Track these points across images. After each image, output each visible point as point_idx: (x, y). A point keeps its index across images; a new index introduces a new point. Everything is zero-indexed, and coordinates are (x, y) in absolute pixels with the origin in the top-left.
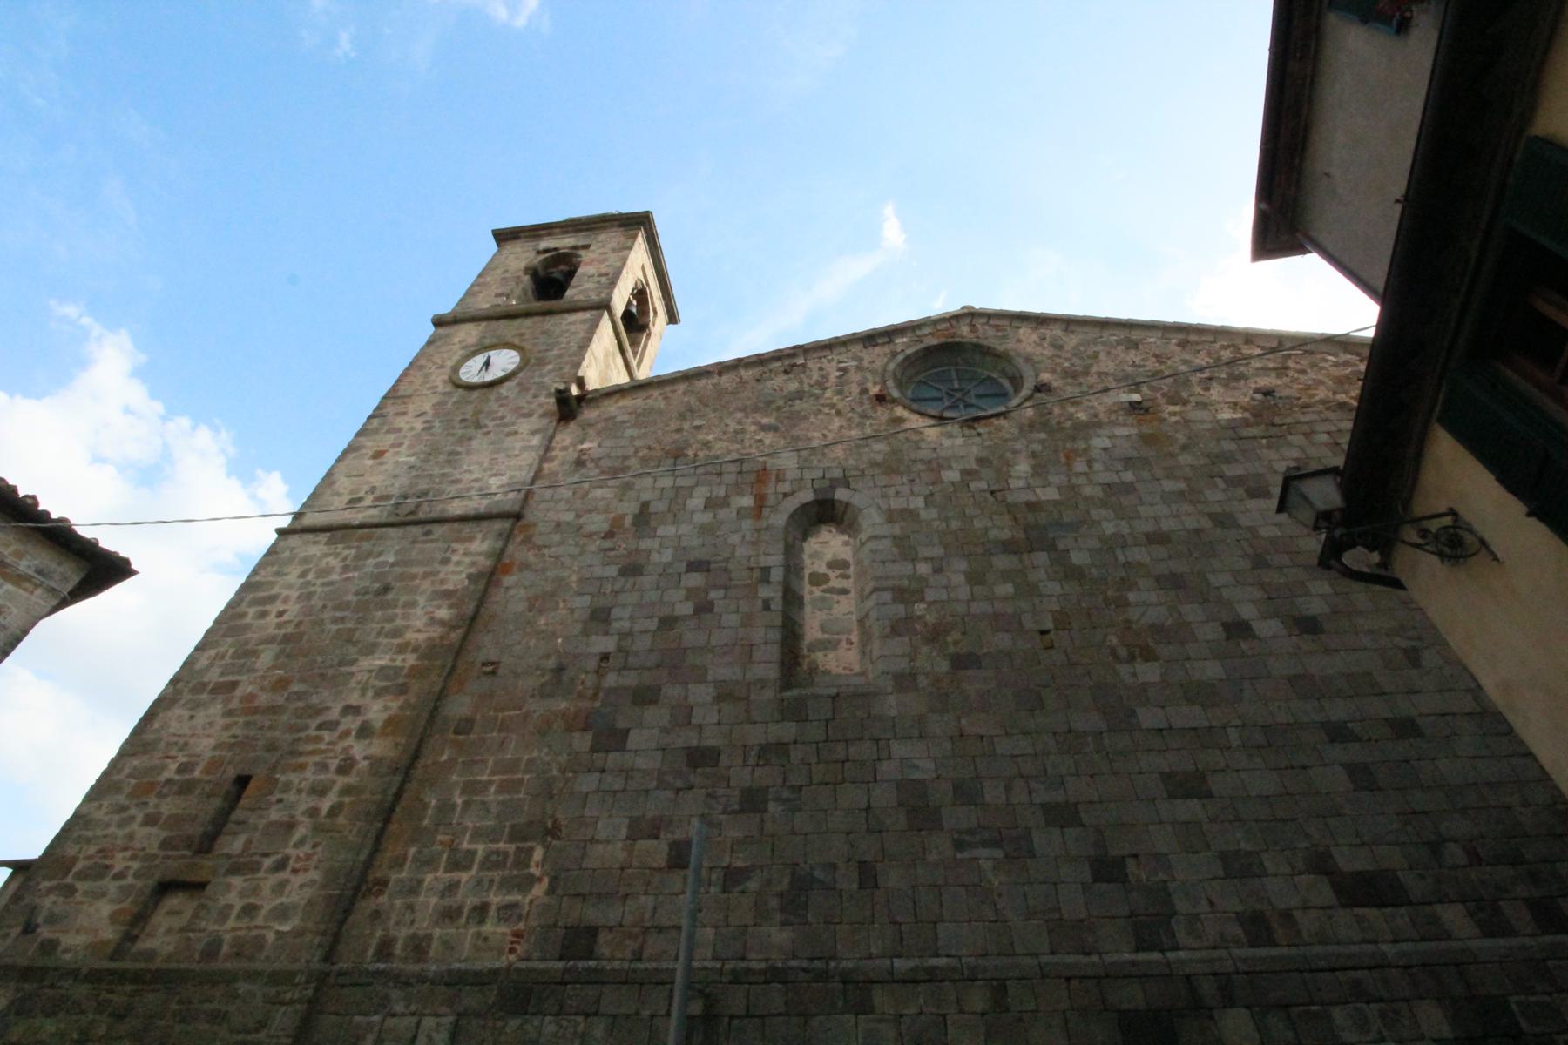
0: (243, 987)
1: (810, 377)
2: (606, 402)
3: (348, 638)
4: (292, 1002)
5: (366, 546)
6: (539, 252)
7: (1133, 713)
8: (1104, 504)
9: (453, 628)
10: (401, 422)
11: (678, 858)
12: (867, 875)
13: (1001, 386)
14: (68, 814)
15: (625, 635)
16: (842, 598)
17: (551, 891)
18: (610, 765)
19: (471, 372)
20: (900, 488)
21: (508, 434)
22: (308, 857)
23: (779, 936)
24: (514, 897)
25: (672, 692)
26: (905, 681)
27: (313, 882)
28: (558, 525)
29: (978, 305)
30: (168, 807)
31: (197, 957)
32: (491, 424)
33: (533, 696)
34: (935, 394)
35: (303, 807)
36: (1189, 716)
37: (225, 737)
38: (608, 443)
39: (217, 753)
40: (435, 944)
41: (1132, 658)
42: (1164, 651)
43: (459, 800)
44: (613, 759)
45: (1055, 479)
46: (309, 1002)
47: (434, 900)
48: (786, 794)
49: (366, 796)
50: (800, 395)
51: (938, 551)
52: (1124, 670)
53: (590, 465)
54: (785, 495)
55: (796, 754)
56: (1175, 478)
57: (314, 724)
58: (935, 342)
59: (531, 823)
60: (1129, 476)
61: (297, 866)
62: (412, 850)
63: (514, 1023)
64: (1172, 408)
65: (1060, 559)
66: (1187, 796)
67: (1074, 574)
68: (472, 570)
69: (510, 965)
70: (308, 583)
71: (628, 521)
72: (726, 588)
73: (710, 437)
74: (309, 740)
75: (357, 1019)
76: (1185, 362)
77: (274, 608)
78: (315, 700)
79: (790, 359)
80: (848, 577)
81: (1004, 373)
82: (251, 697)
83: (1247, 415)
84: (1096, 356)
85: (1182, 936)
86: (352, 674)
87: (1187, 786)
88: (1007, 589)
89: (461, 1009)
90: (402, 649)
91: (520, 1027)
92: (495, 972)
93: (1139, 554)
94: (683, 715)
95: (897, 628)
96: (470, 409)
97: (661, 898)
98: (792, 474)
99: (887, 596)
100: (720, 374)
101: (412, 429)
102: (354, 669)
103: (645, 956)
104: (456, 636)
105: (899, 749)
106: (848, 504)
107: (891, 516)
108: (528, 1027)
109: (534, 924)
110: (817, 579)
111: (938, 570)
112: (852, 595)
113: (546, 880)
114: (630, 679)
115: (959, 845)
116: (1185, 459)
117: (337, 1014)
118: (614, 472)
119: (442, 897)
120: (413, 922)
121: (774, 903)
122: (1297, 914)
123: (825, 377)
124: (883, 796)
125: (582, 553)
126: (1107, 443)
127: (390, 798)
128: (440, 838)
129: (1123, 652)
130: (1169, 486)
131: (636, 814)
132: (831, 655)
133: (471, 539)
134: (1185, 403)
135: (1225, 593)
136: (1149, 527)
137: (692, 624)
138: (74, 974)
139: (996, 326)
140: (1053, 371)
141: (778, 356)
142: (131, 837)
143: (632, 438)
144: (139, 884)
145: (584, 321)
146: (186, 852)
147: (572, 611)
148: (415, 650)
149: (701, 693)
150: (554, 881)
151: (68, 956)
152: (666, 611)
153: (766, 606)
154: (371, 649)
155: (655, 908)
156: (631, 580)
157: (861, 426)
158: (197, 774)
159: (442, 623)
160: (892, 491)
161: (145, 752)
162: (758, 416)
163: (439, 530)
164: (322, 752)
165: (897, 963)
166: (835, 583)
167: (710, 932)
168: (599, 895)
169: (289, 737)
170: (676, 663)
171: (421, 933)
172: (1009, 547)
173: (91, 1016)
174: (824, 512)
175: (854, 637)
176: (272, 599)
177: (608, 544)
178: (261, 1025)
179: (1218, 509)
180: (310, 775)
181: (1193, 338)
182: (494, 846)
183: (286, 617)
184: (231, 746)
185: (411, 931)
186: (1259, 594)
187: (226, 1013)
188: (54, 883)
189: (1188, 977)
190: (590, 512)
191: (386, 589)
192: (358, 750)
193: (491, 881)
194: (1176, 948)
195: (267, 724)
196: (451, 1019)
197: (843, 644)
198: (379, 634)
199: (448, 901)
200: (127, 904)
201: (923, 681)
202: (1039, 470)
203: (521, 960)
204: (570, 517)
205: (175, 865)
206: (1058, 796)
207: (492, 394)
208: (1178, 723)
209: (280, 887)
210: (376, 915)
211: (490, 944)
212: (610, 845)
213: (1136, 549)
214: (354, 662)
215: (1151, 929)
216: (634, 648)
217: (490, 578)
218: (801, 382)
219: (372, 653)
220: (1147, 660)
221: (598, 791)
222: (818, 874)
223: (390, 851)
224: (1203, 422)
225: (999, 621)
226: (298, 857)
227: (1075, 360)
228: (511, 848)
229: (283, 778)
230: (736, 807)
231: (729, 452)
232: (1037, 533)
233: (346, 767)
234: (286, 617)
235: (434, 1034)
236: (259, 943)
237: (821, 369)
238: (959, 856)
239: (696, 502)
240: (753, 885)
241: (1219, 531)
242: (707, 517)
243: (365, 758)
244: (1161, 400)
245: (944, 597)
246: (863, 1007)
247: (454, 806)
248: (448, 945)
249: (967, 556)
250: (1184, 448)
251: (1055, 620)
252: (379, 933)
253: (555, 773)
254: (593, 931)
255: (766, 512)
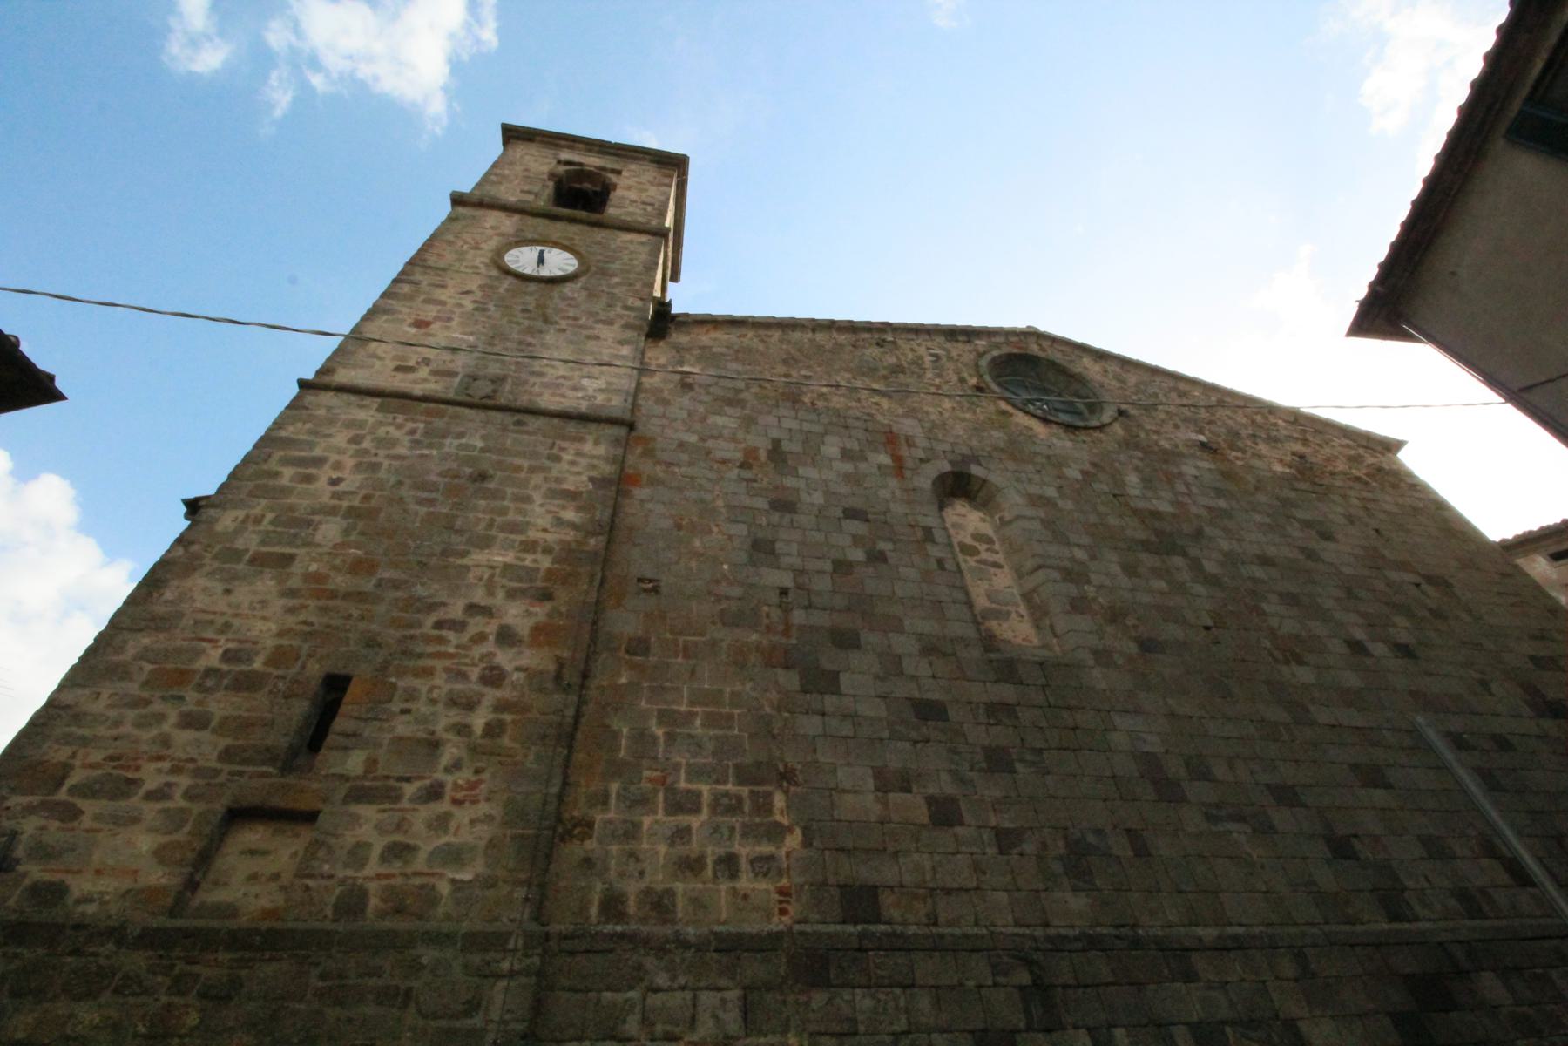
0: (428, 955)
2: (697, 330)
4: (512, 974)
6: (559, 162)
9: (590, 534)
11: (944, 813)
14: (40, 701)
15: (799, 572)
17: (807, 842)
19: (523, 259)
21: (589, 337)
22: (472, 786)
23: (1078, 903)
24: (766, 849)
26: (1103, 656)
27: (489, 818)
29: (1042, 328)
30: (220, 705)
31: (329, 912)
33: (713, 623)
35: (443, 723)
39: (285, 642)
40: (681, 903)
43: (660, 732)
44: (830, 702)
46: (539, 974)
47: (662, 849)
52: (1285, 670)
55: (1026, 716)
57: (431, 620)
61: (460, 795)
62: (614, 787)
63: (819, 998)
66: (1376, 786)
67: (1212, 581)
70: (366, 452)
74: (428, 639)
77: (325, 473)
78: (420, 591)
82: (318, 578)
86: (467, 568)
88: (1161, 584)
90: (529, 547)
92: (776, 937)
94: (893, 666)
100: (814, 331)
101: (460, 306)
102: (465, 561)
103: (941, 920)
106: (985, 481)
109: (799, 880)
110: (968, 550)
112: (1006, 569)
113: (798, 832)
116: (1262, 498)
119: (672, 844)
120: (642, 873)
121: (1057, 867)
132: (1005, 625)
133: (581, 440)
138: (117, 934)
142: (166, 741)
144: (197, 808)
146: (271, 769)
151: (91, 909)
154: (485, 543)
155: (933, 868)
158: (257, 664)
159: (573, 526)
161: (157, 629)
163: (534, 423)
164: (452, 656)
168: (867, 851)
169: (399, 634)
171: (659, 887)
173: (164, 999)
176: (319, 462)
177: (747, 474)
178: (472, 1007)
180: (442, 684)
182: (722, 787)
183: (342, 487)
184: (306, 636)
187: (409, 991)
188: (35, 799)
190: (716, 438)
191: (483, 477)
193: (732, 829)
195: (356, 613)
198: (490, 525)
199: (681, 850)
200: (181, 836)
202: (1147, 482)
205: (257, 784)
207: (556, 291)
209: (442, 823)
215: (1393, 903)
217: (620, 483)
219: (488, 547)
221: (825, 735)
222: (1091, 838)
226: (456, 786)
228: (745, 791)
229: (401, 684)
233: (493, 677)
234: (342, 487)
235: (721, 1014)
236: (429, 896)
237: (912, 350)
239: (831, 448)
240: (1029, 847)
243: (518, 669)
246: (1190, 977)
247: (654, 739)
248: (697, 903)
253: (768, 709)
254: (873, 891)
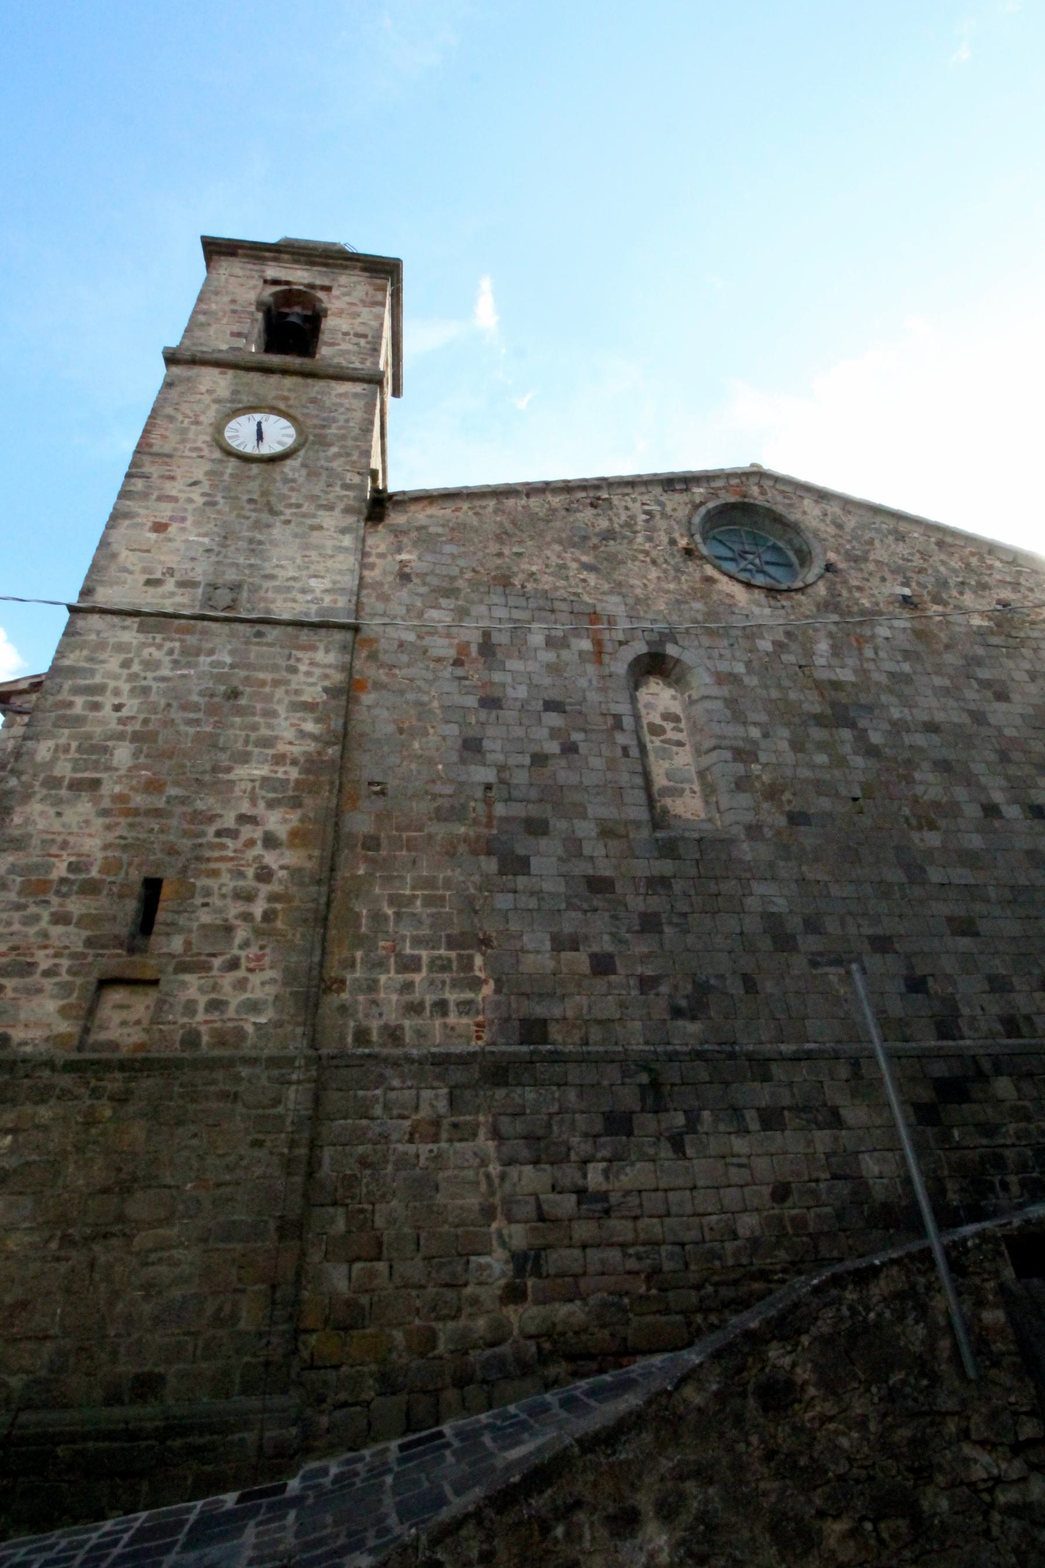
0: (245, 1072)
1: (617, 515)
2: (413, 508)
3: (212, 743)
4: (299, 1082)
5: (191, 640)
7: (924, 871)
8: (891, 691)
10: (172, 489)
12: (750, 984)
13: (787, 557)
15: (502, 768)
16: (679, 749)
17: (498, 990)
18: (520, 887)
20: (723, 652)
22: (259, 958)
24: (469, 995)
25: (559, 825)
26: (754, 831)
27: (273, 981)
28: (401, 645)
32: (288, 511)
34: (729, 554)
36: (960, 875)
37: (110, 837)
38: (429, 557)
41: (920, 828)
42: (942, 823)
44: (522, 881)
45: (850, 662)
47: (394, 997)
48: (675, 920)
49: (296, 903)
50: (609, 535)
51: (764, 718)
52: (915, 836)
53: (416, 580)
54: (621, 643)
55: (678, 886)
56: (942, 675)
57: (211, 830)
58: (732, 499)
59: (463, 934)
60: (906, 667)
62: (359, 954)
64: (936, 607)
65: (861, 736)
67: (873, 752)
68: (327, 683)
69: (483, 1049)
71: (474, 650)
72: (585, 731)
73: (534, 568)
74: (212, 846)
75: (361, 1093)
76: (943, 563)
78: (200, 805)
79: (595, 492)
80: (681, 731)
81: (790, 542)
83: (992, 624)
84: (871, 542)
85: (966, 1031)
86: (233, 782)
87: (965, 927)
88: (821, 758)
89: (452, 1083)
91: (507, 1095)
92: (474, 1054)
93: (920, 739)
94: (574, 847)
95: (741, 784)
96: (254, 485)
97: (593, 998)
98: (623, 624)
99: (728, 755)
100: (528, 495)
104: (332, 752)
105: (759, 888)
106: (678, 661)
107: (721, 679)
108: (513, 1095)
110: (656, 730)
111: (766, 735)
112: (688, 747)
113: (492, 983)
114: (518, 810)
115: (814, 964)
117: (340, 1090)
118: (450, 592)
120: (381, 1015)
122: (1035, 1018)
123: (632, 517)
124: (753, 925)
125: (436, 679)
126: (887, 633)
127: (322, 907)
128: (382, 944)
129: (914, 822)
130: (938, 681)
131: (556, 929)
133: (313, 648)
134: (945, 604)
135: (983, 780)
136: (925, 717)
137: (563, 763)
139: (783, 492)
140: (838, 552)
141: (584, 485)
142: (45, 935)
143: (453, 556)
144: (79, 981)
145: (356, 395)
146: (119, 951)
147: (444, 738)
148: (294, 762)
149: (586, 829)
150: (498, 981)
152: (536, 748)
153: (625, 750)
156: (494, 713)
157: (677, 579)
159: (315, 738)
160: (715, 653)
162: (578, 553)
163: (273, 633)
164: (232, 859)
165: (783, 1047)
166: (671, 735)
167: (638, 1024)
168: (540, 995)
170: (553, 795)
172: (819, 720)
174: (655, 665)
175: (697, 787)
177: (460, 672)
178: (277, 1101)
179: (973, 706)
181: (949, 540)
182: (436, 952)
184: (125, 848)
185: (382, 1023)
186: (1004, 783)
189: (974, 1057)
192: (271, 859)
193: (444, 983)
194: (962, 1038)
196: (445, 1090)
197: (688, 792)
199: (408, 998)
200: (73, 999)
201: (768, 833)
202: (836, 651)
203: (488, 1044)
204: (411, 637)
206: (879, 931)
208: (956, 881)
209: (241, 985)
210: (343, 1009)
211: (459, 1031)
212: (538, 957)
213: (917, 735)
214: (229, 770)
215: (946, 1026)
216: (515, 781)
217: (348, 691)
218: (610, 520)
219: (247, 762)
220: (931, 830)
221: (516, 909)
222: (712, 982)
223: (338, 954)
224: (960, 625)
225: (821, 787)
227: (854, 543)
228: (453, 954)
230: (637, 928)
231: (556, 589)
232: (841, 711)
233: (264, 875)
235: (435, 1103)
236: (240, 1034)
237: (627, 508)
238: (814, 972)
239: (537, 639)
240: (664, 989)
241: (975, 727)
242: (549, 656)
243: (282, 867)
244: (927, 598)
245: (774, 761)
247: (386, 918)
249: (788, 725)
250: (947, 647)
251: (863, 789)
252: (352, 1024)
253: (472, 891)
254: (544, 1023)
255: (606, 658)
